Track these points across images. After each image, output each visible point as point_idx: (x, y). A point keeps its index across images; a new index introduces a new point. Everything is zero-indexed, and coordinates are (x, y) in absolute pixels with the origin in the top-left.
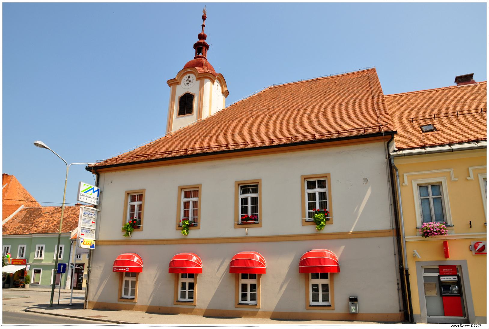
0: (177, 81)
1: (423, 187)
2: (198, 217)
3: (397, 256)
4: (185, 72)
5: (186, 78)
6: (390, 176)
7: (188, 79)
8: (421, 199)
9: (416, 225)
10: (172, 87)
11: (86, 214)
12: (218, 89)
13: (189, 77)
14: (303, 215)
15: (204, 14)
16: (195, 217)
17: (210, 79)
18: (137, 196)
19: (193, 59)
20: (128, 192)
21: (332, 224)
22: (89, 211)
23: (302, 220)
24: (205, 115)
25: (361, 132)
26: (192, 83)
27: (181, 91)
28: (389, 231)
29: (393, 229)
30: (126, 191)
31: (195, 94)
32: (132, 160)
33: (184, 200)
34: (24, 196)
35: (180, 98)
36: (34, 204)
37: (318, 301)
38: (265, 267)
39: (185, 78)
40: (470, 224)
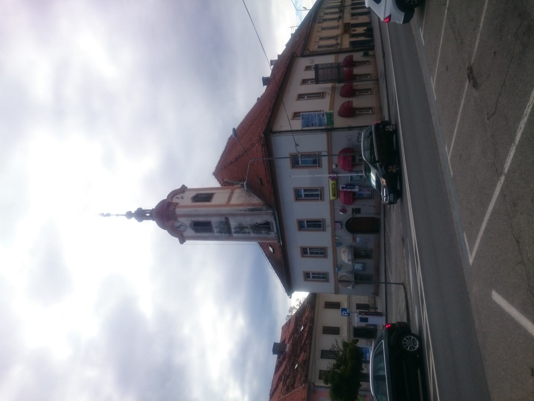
11: (307, 124)
17: (174, 209)
18: (298, 196)
22: (304, 121)
28: (328, 135)
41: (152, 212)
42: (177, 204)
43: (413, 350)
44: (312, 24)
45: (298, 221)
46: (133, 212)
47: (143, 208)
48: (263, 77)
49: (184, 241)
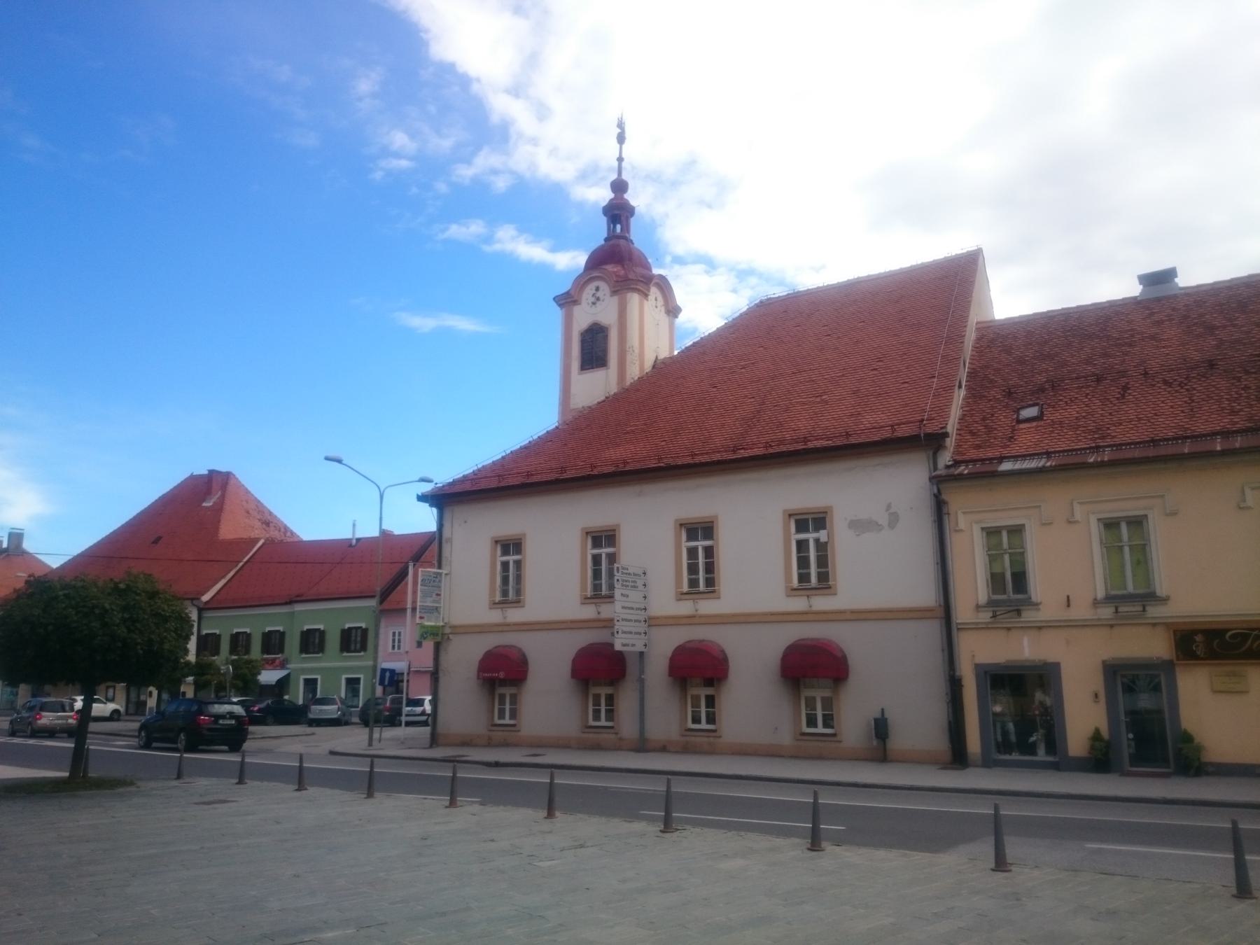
0: (573, 297)
1: (992, 533)
2: (716, 575)
3: (946, 653)
8: (989, 555)
9: (977, 598)
12: (656, 307)
13: (597, 289)
14: (584, 588)
15: (620, 131)
16: (505, 588)
17: (638, 291)
18: (511, 546)
19: (603, 242)
20: (496, 539)
21: (836, 594)
23: (676, 592)
24: (633, 373)
25: (886, 434)
27: (584, 317)
29: (940, 605)
30: (493, 538)
31: (610, 325)
32: (500, 482)
33: (591, 552)
34: (259, 517)
35: (582, 334)
36: (282, 534)
37: (816, 726)
38: (256, 540)
39: (590, 290)
41: (624, 237)
42: (646, 295)
43: (268, 704)
44: (1159, 624)
45: (521, 539)
46: (626, 196)
47: (633, 220)
48: (418, 495)
49: (561, 305)
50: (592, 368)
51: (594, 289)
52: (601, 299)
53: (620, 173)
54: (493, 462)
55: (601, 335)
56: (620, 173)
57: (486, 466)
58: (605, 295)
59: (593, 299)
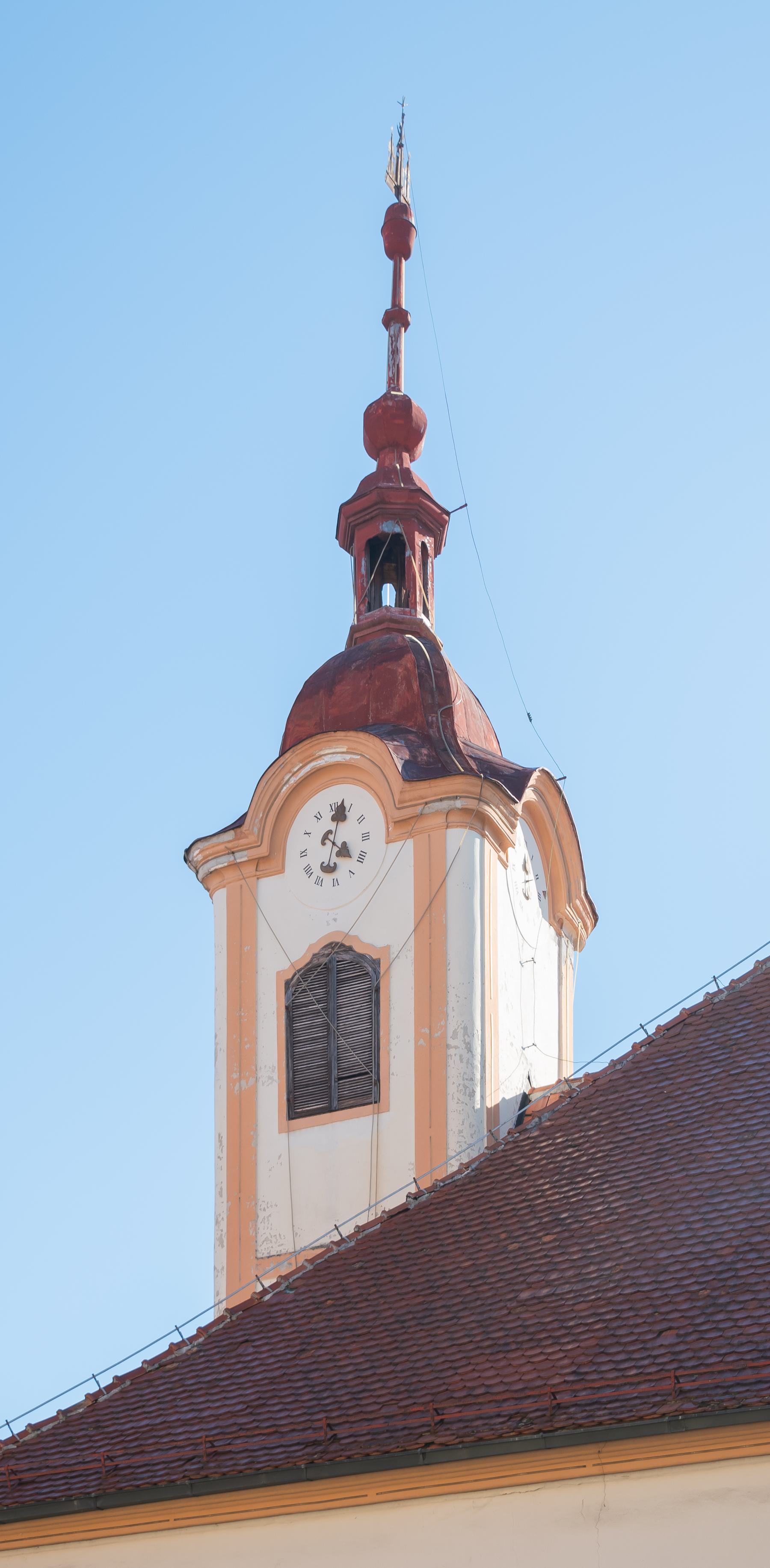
4: (308, 768)
5: (318, 817)
6: (454, 977)
7: (332, 826)
10: (221, 894)
13: (340, 814)
26: (361, 859)
31: (388, 948)
35: (287, 984)
40: (529, 1078)
50: (329, 1110)
51: (328, 814)
52: (355, 852)
53: (394, 380)
54: (613, 1063)
55: (358, 986)
56: (394, 380)
57: (620, 1060)
58: (366, 837)
59: (325, 854)
